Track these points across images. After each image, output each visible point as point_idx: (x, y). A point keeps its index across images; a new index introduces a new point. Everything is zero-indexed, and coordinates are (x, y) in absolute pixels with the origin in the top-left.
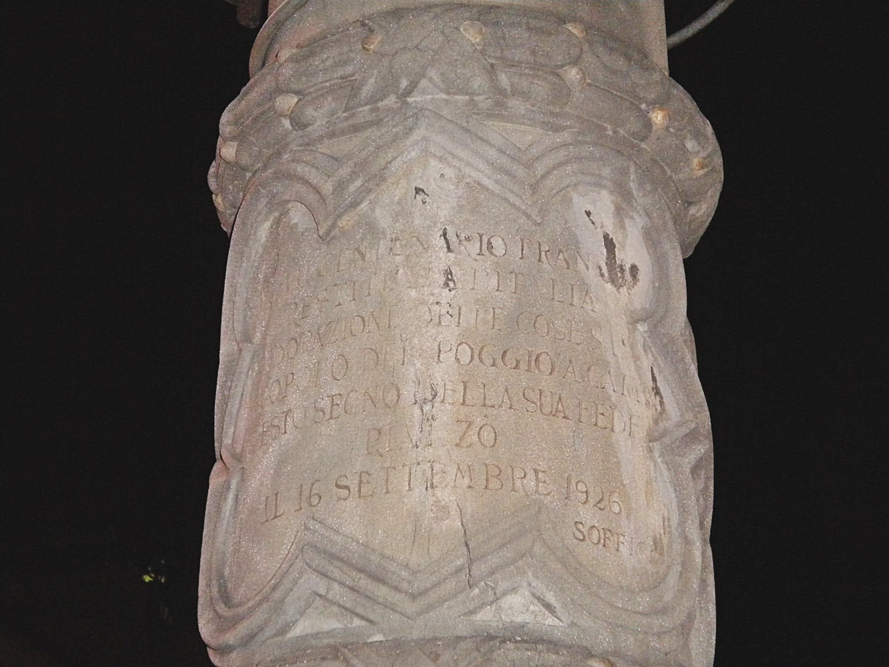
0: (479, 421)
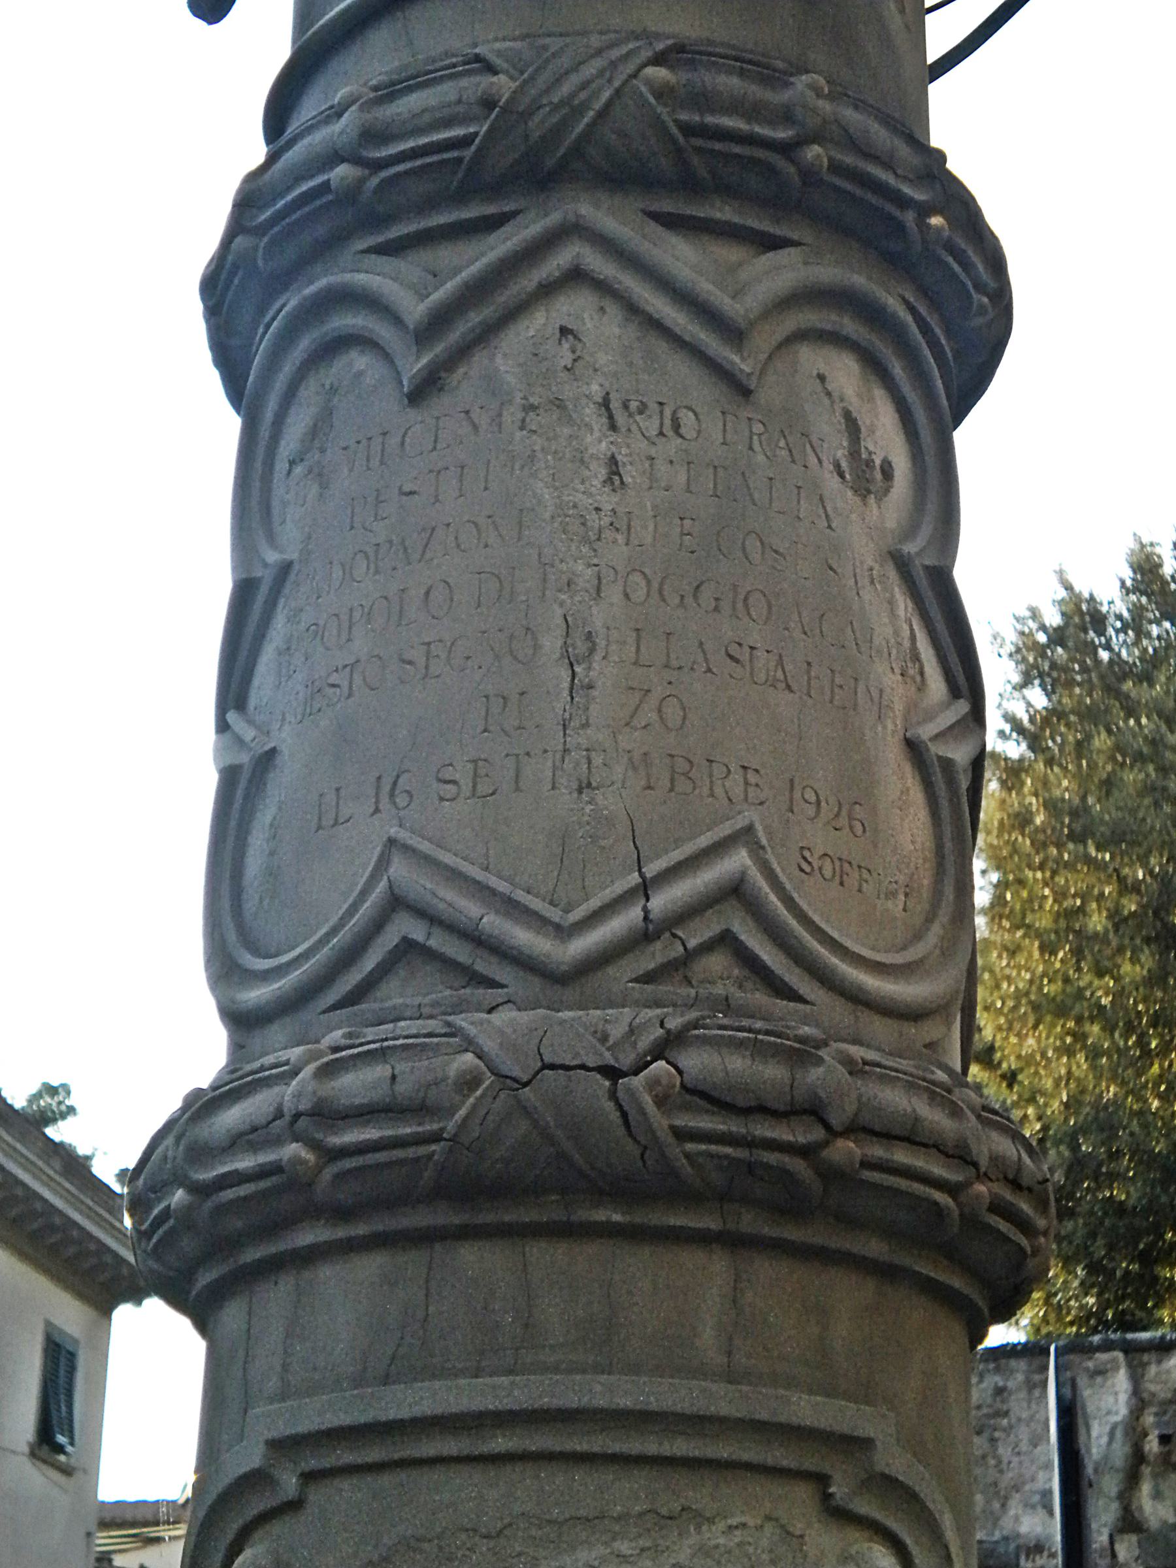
0: (658, 692)
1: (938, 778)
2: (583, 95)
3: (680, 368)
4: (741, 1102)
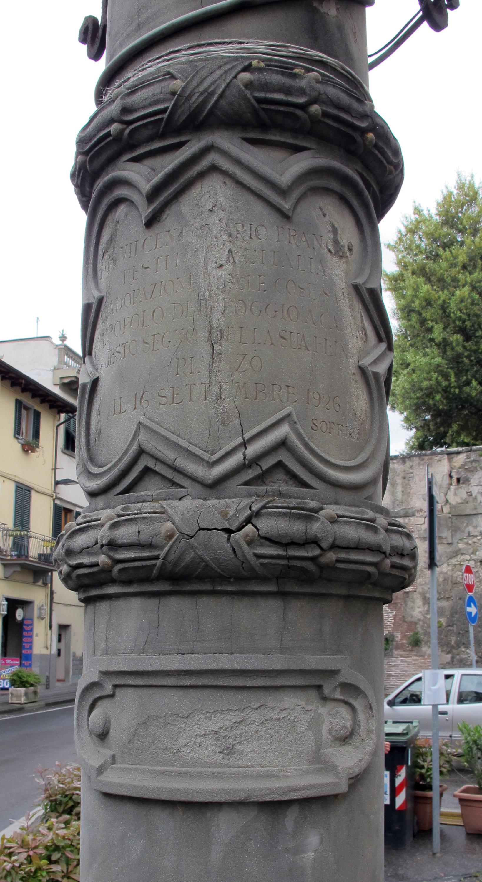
1: (373, 382)
2: (212, 88)
3: (259, 207)
4: (284, 541)
